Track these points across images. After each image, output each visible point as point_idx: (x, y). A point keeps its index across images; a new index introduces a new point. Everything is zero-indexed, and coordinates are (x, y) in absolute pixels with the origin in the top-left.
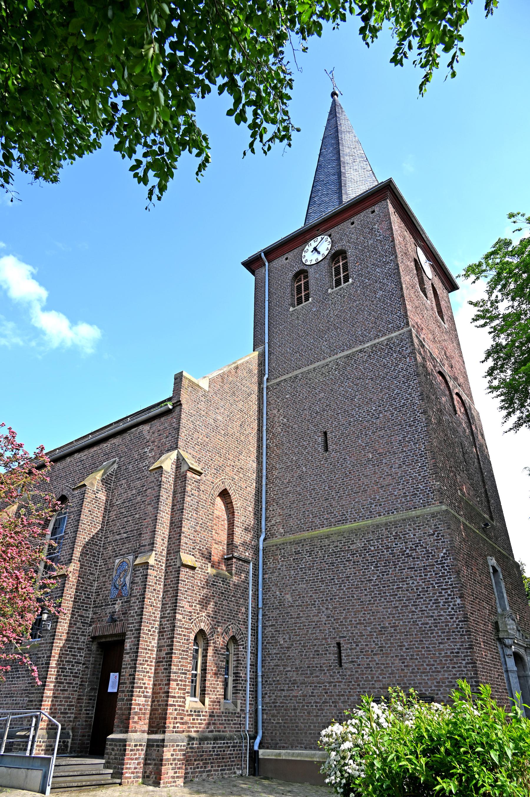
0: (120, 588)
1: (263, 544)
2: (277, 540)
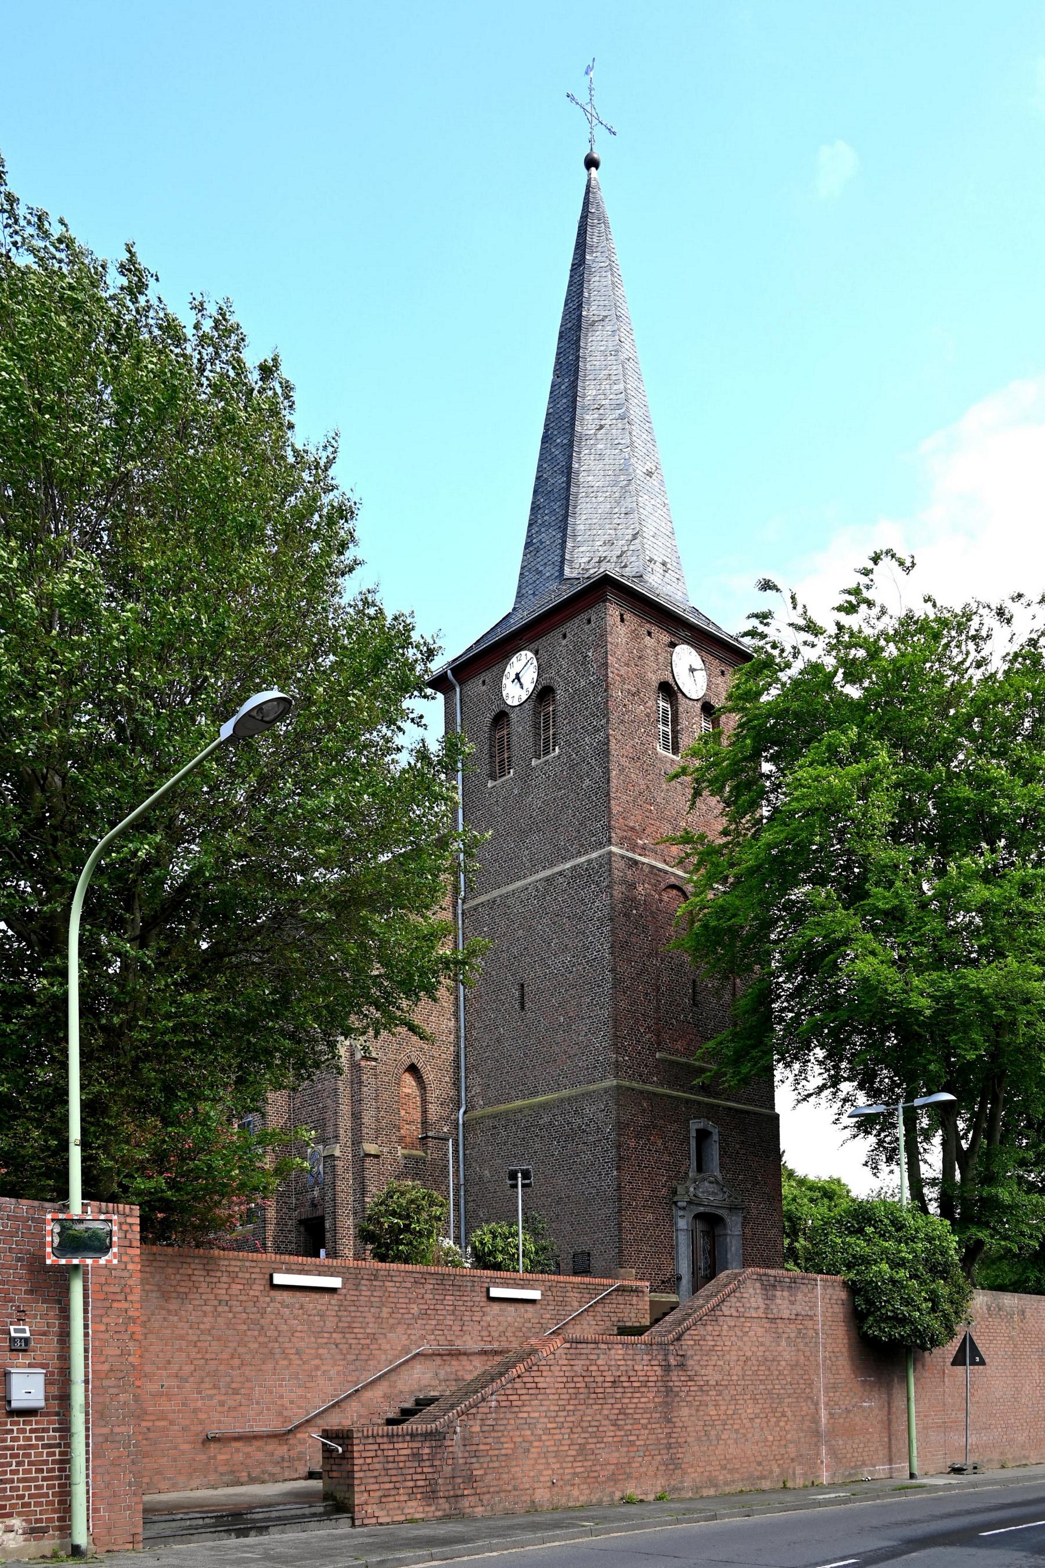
2: (477, 1113)
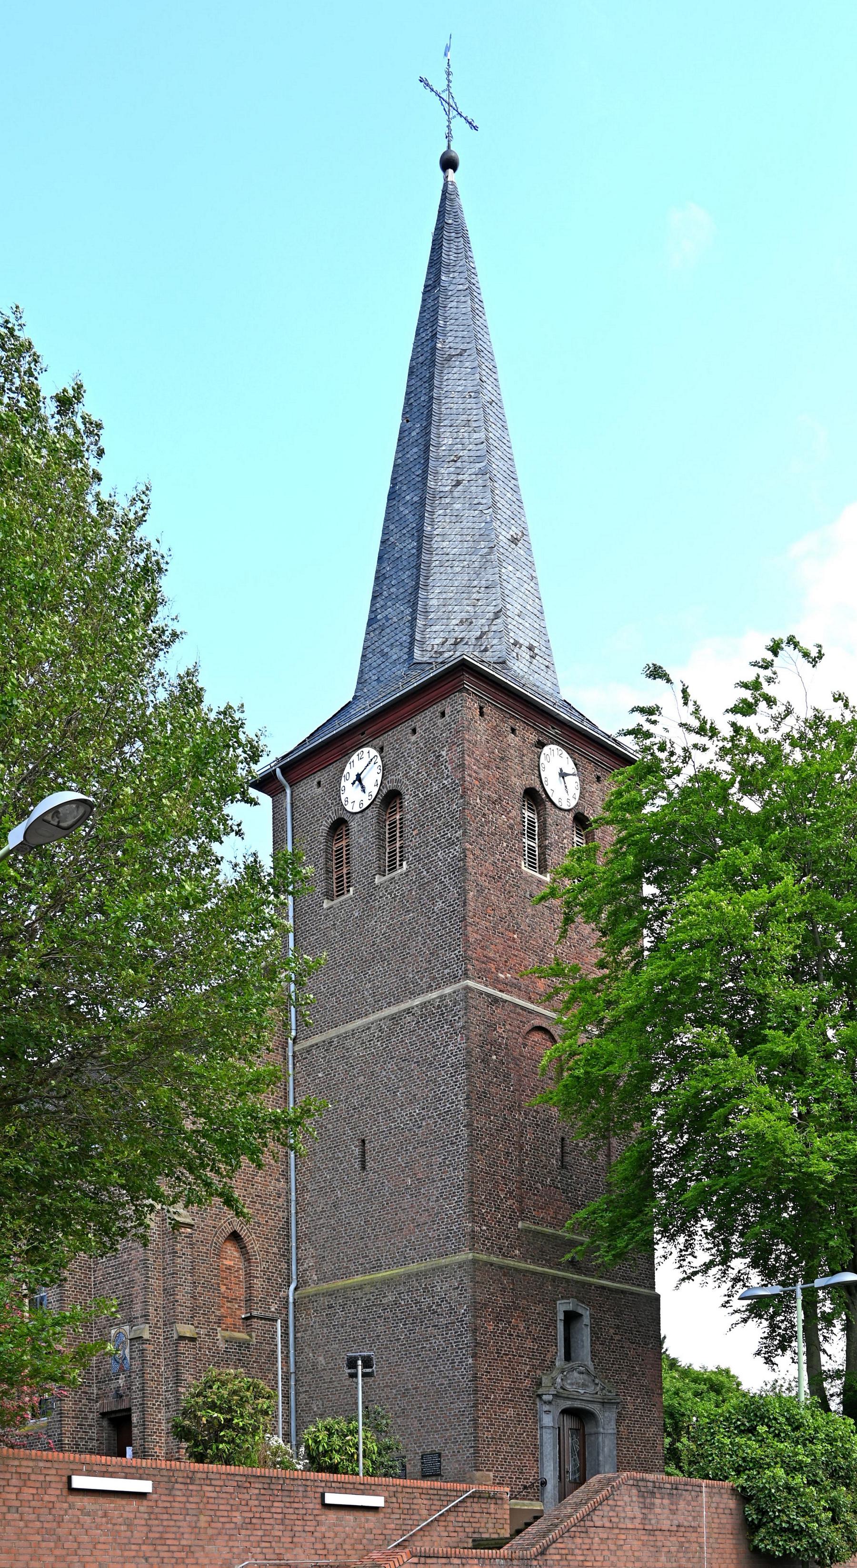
0: (120, 1361)
1: (294, 1295)
2: (311, 1289)
